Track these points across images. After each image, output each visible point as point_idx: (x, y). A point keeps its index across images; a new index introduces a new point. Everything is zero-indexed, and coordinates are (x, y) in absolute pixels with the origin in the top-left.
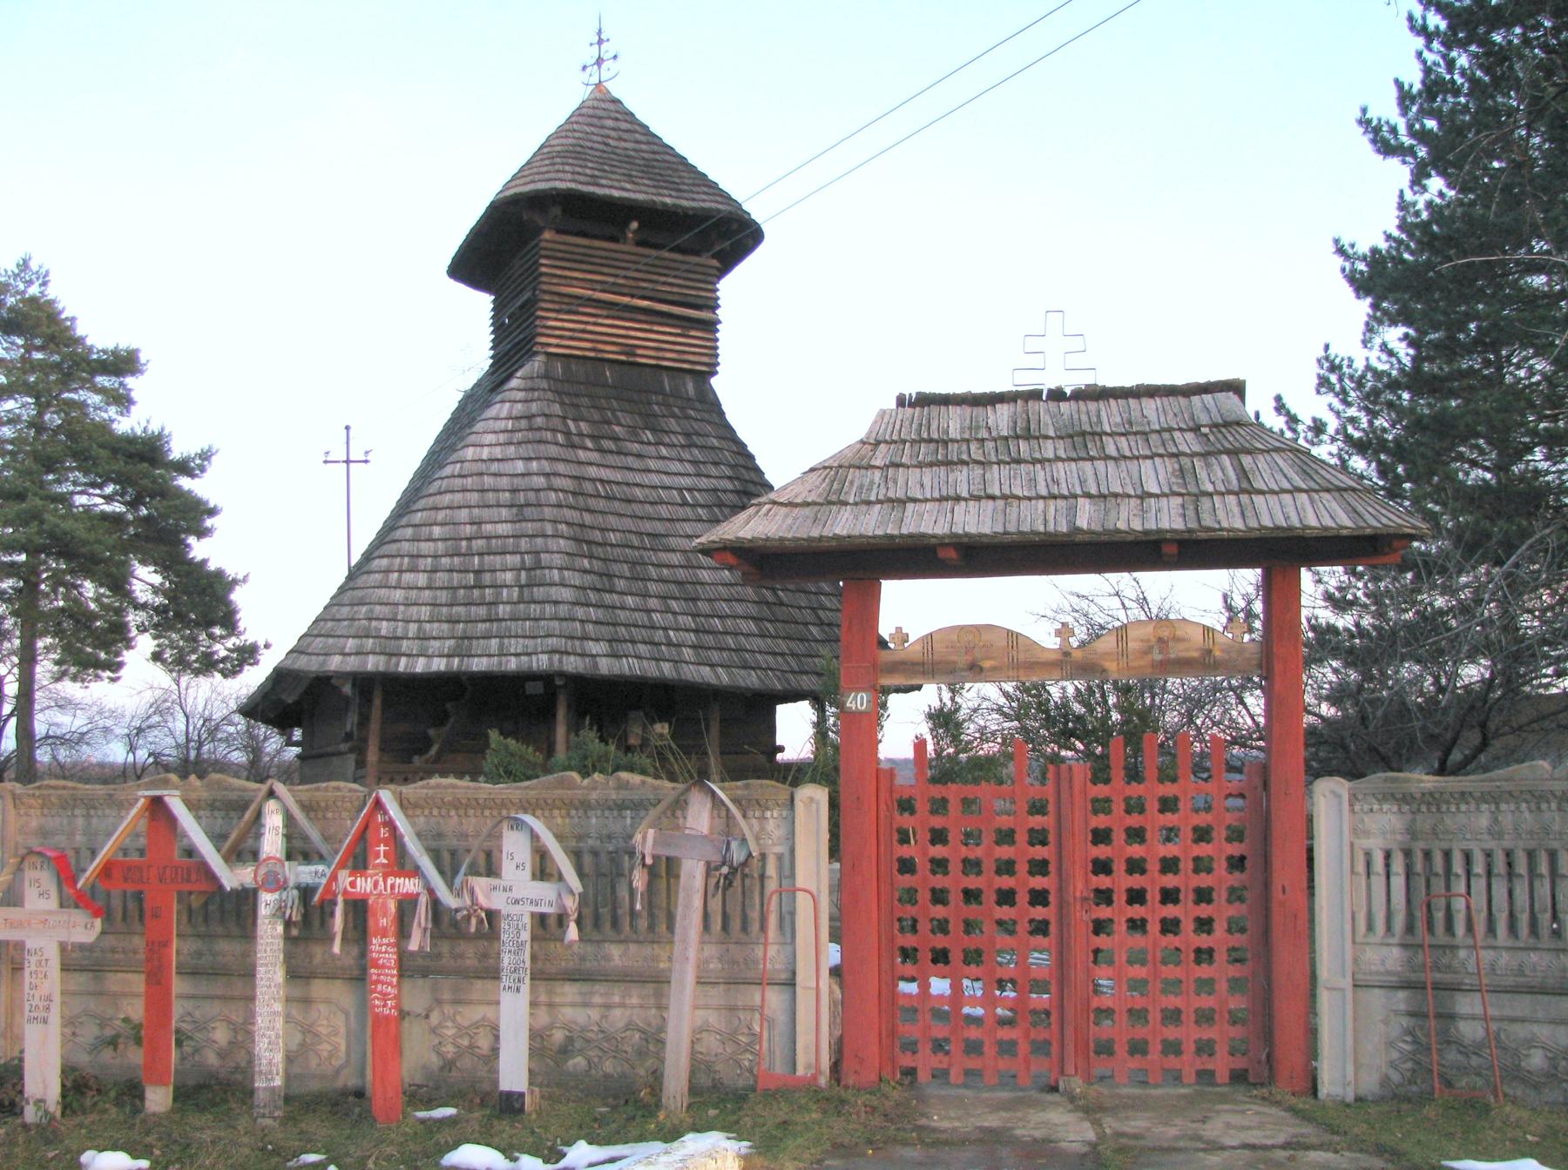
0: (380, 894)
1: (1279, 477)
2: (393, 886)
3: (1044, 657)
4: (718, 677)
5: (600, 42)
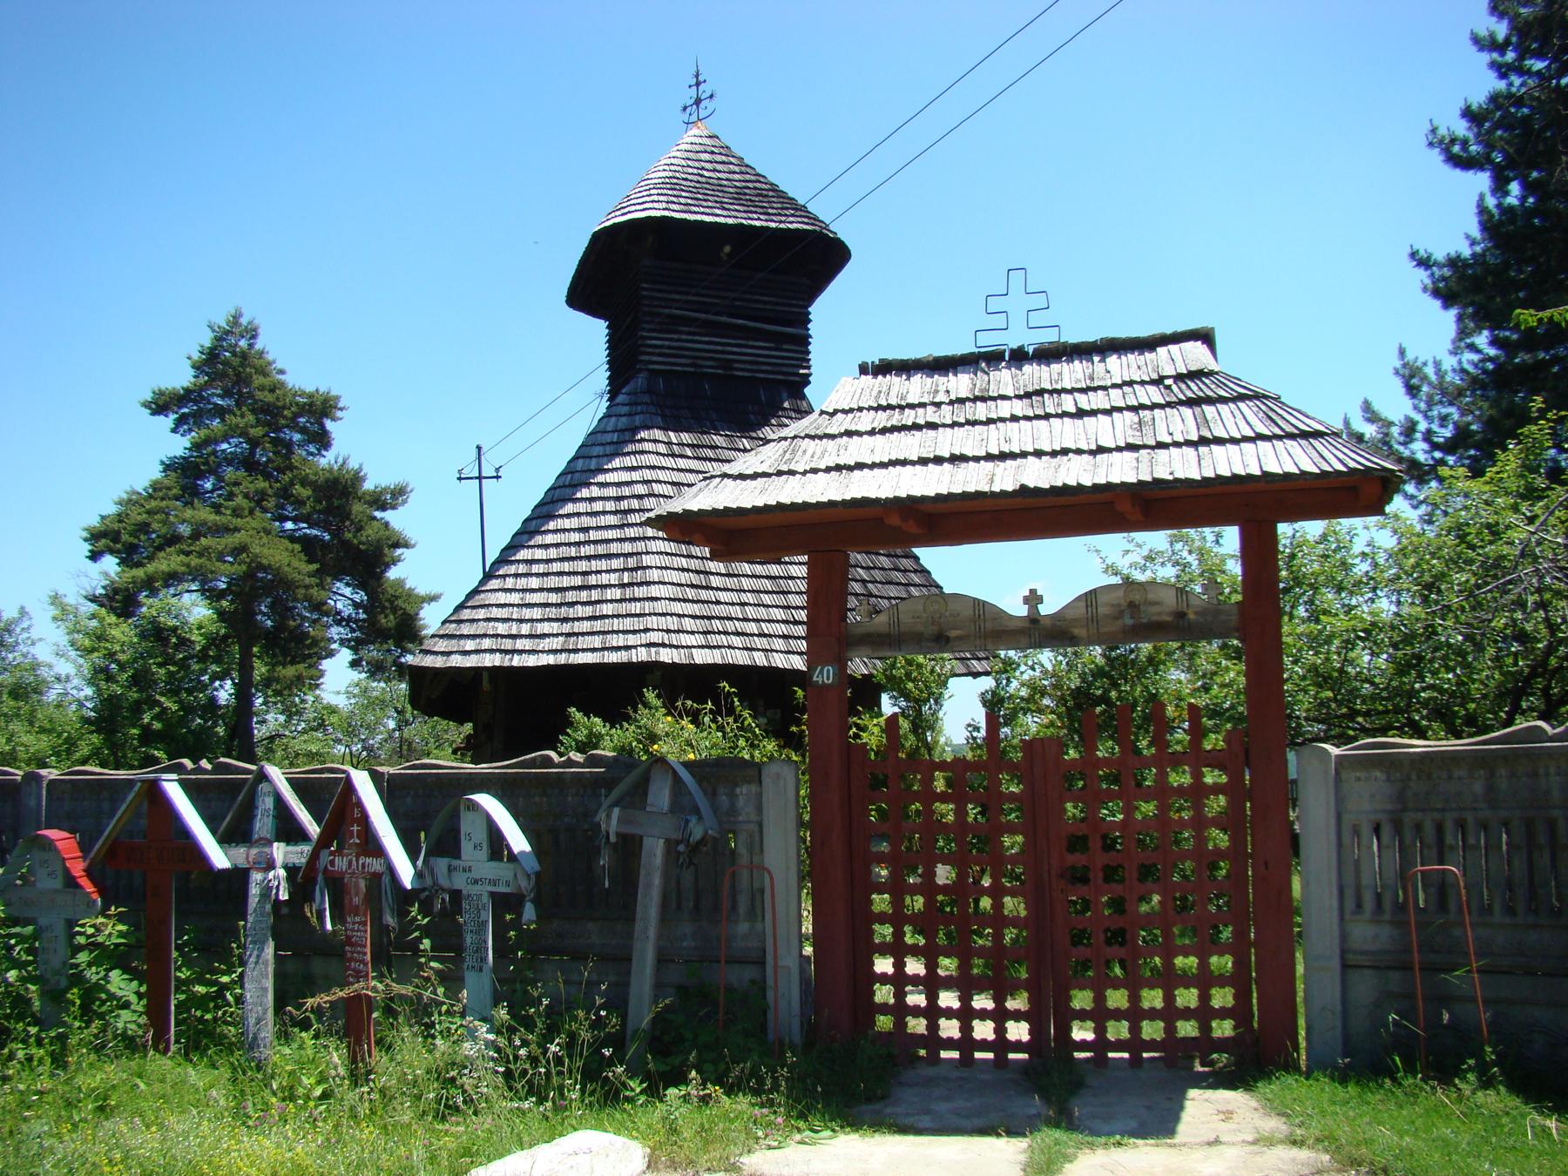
1: (1242, 424)
3: (1011, 625)
5: (698, 84)
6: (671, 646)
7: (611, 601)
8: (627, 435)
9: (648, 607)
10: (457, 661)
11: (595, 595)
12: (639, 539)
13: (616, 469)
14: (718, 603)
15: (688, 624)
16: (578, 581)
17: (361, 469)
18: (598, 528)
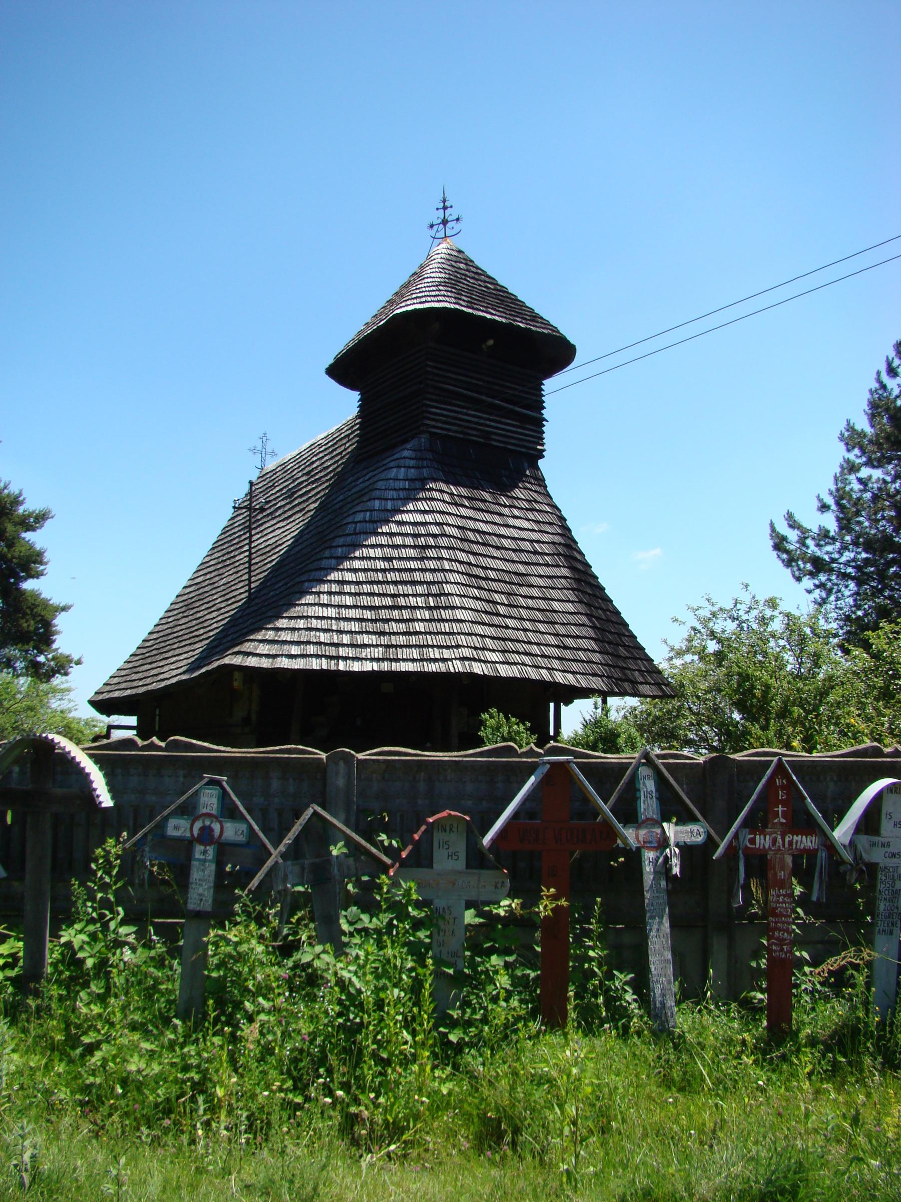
0: (779, 849)
2: (790, 843)
4: (578, 682)
5: (445, 208)
6: (480, 661)
7: (422, 620)
8: (418, 484)
9: (456, 627)
10: (284, 663)
11: (406, 614)
12: (438, 570)
13: (411, 511)
14: (507, 627)
15: (489, 643)
16: (389, 601)
17: (20, 494)
18: (400, 559)
